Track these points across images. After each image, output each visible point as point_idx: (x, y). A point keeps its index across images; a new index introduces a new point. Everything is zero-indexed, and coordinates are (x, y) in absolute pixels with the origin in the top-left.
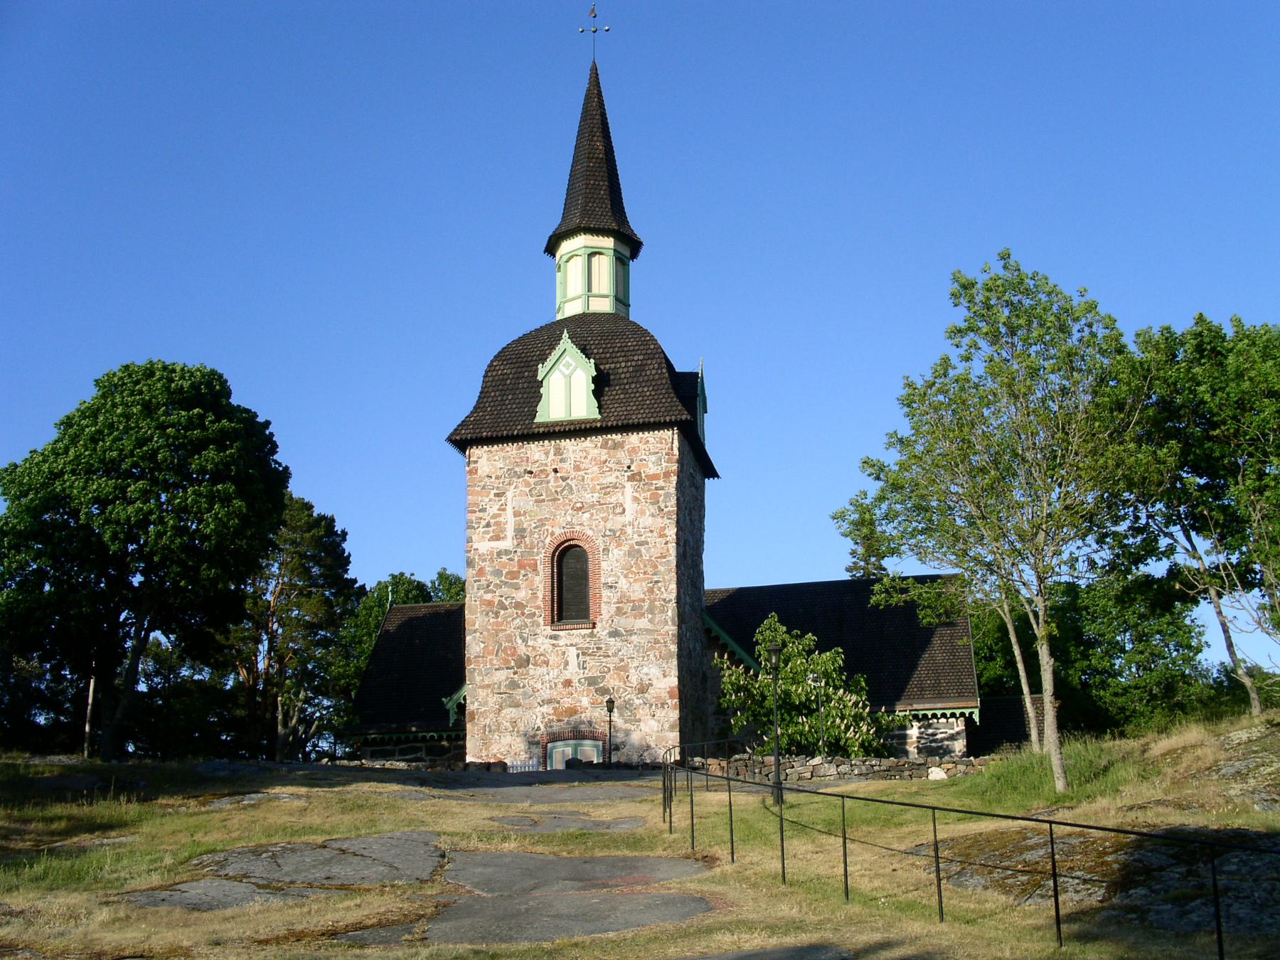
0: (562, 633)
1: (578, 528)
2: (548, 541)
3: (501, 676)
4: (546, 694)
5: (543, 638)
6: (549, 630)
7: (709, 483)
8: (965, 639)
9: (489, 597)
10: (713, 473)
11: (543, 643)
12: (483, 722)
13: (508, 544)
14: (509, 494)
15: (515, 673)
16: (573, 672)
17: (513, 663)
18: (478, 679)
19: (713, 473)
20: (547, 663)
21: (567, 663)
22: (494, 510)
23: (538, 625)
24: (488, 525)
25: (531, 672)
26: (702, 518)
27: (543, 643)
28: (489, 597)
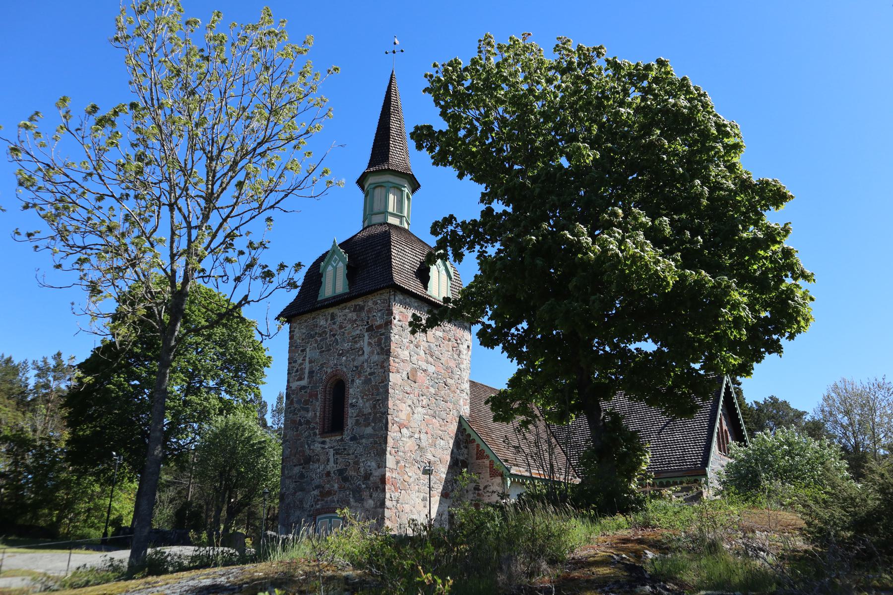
0: (327, 440)
20: (318, 460)
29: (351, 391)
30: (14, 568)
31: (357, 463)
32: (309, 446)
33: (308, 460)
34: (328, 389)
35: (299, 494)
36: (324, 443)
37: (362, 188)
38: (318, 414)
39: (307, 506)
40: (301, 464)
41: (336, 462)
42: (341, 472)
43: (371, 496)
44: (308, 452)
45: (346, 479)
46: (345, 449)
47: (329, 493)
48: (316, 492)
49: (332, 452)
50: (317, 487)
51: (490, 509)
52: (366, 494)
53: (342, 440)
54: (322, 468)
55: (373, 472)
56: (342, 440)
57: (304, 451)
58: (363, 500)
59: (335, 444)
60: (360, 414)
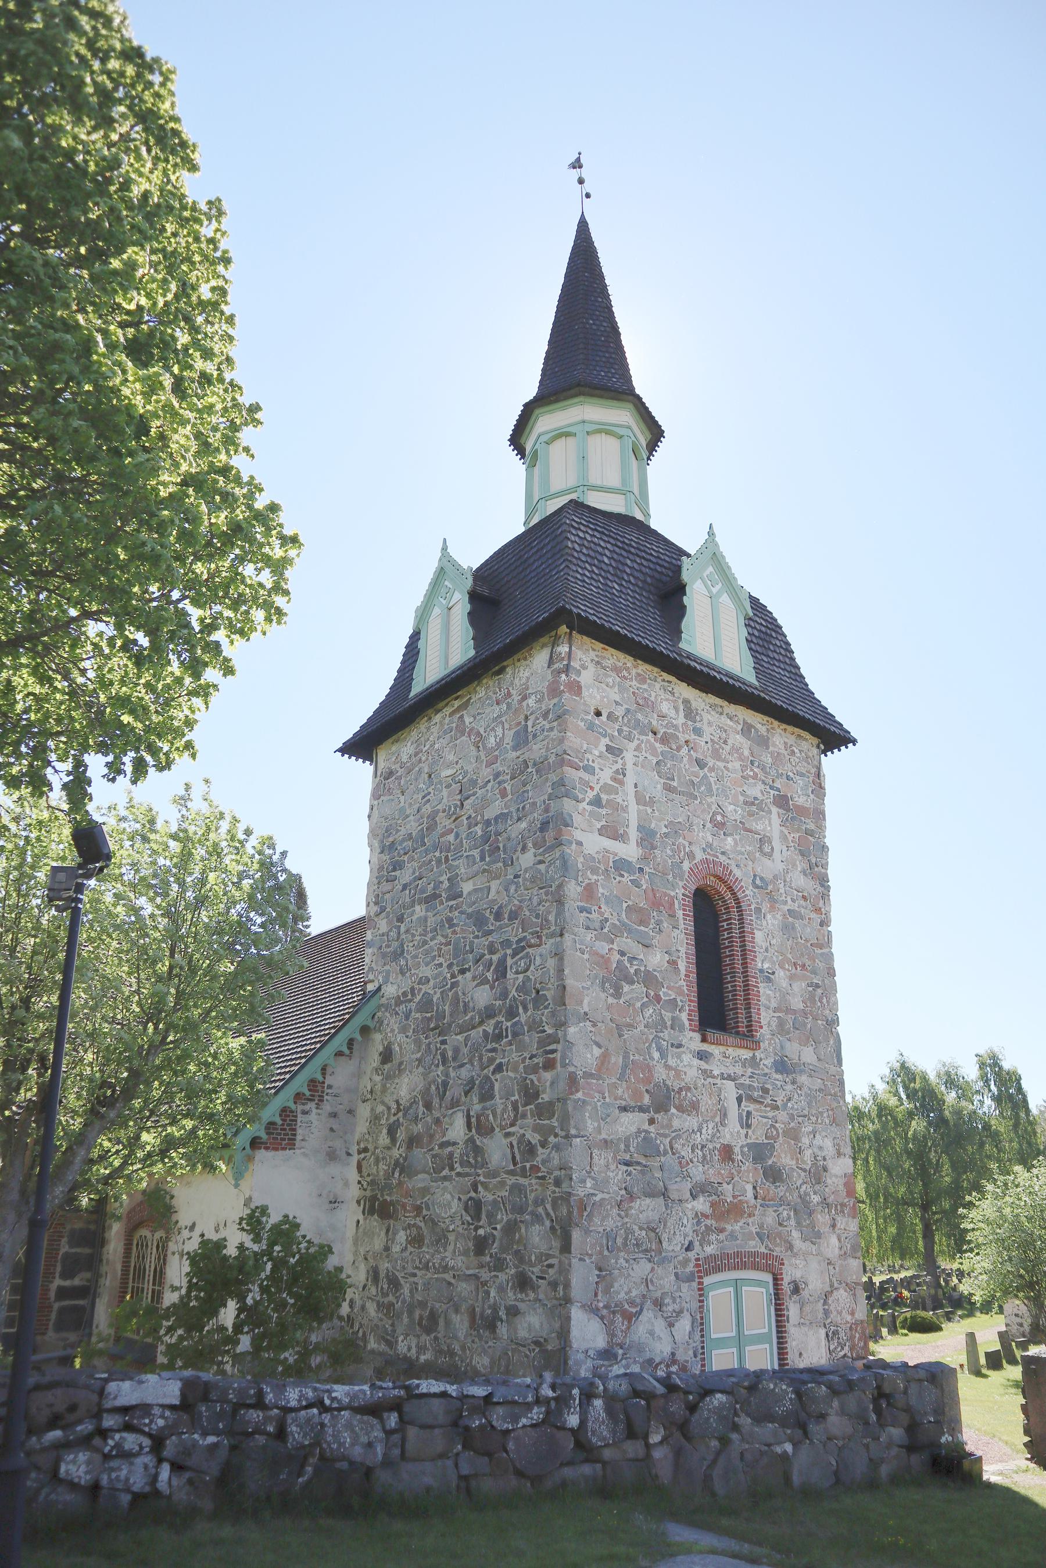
0: (715, 1050)
1: (722, 859)
2: (686, 866)
3: (630, 1123)
4: (698, 1172)
5: (691, 1060)
6: (692, 1040)
7: (833, 763)
8: (292, 1301)
9: (603, 947)
10: (833, 737)
11: (689, 1067)
12: (598, 1225)
13: (630, 851)
14: (629, 756)
15: (652, 1122)
16: (732, 1133)
17: (646, 1100)
18: (590, 1125)
19: (833, 737)
20: (695, 1106)
21: (725, 1115)
22: (605, 776)
23: (682, 1029)
24: (597, 802)
25: (676, 1123)
26: (628, 370)
27: (689, 1067)
28: (603, 947)
29: (759, 936)
30: (744, 633)
31: (793, 1135)
32: (663, 1055)
33: (662, 1100)
34: (735, 914)
35: (647, 1209)
36: (702, 1056)
37: (521, 451)
38: (682, 966)
39: (673, 1245)
40: (642, 1109)
41: (746, 1122)
42: (759, 1153)
43: (834, 1226)
44: (660, 1074)
45: (774, 1175)
46: (766, 1091)
47: (736, 1210)
48: (701, 1204)
49: (730, 1091)
50: (698, 1190)
51: (859, 1162)
52: (822, 1219)
53: (753, 1062)
54: (708, 1130)
55: (830, 1164)
56: (753, 1062)
57: (650, 1069)
58: (819, 1235)
59: (738, 1070)
60: (784, 1008)
